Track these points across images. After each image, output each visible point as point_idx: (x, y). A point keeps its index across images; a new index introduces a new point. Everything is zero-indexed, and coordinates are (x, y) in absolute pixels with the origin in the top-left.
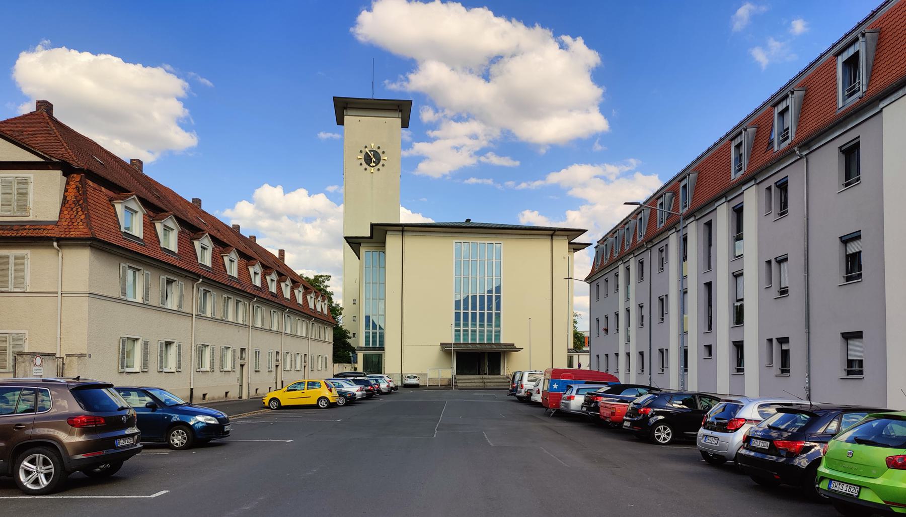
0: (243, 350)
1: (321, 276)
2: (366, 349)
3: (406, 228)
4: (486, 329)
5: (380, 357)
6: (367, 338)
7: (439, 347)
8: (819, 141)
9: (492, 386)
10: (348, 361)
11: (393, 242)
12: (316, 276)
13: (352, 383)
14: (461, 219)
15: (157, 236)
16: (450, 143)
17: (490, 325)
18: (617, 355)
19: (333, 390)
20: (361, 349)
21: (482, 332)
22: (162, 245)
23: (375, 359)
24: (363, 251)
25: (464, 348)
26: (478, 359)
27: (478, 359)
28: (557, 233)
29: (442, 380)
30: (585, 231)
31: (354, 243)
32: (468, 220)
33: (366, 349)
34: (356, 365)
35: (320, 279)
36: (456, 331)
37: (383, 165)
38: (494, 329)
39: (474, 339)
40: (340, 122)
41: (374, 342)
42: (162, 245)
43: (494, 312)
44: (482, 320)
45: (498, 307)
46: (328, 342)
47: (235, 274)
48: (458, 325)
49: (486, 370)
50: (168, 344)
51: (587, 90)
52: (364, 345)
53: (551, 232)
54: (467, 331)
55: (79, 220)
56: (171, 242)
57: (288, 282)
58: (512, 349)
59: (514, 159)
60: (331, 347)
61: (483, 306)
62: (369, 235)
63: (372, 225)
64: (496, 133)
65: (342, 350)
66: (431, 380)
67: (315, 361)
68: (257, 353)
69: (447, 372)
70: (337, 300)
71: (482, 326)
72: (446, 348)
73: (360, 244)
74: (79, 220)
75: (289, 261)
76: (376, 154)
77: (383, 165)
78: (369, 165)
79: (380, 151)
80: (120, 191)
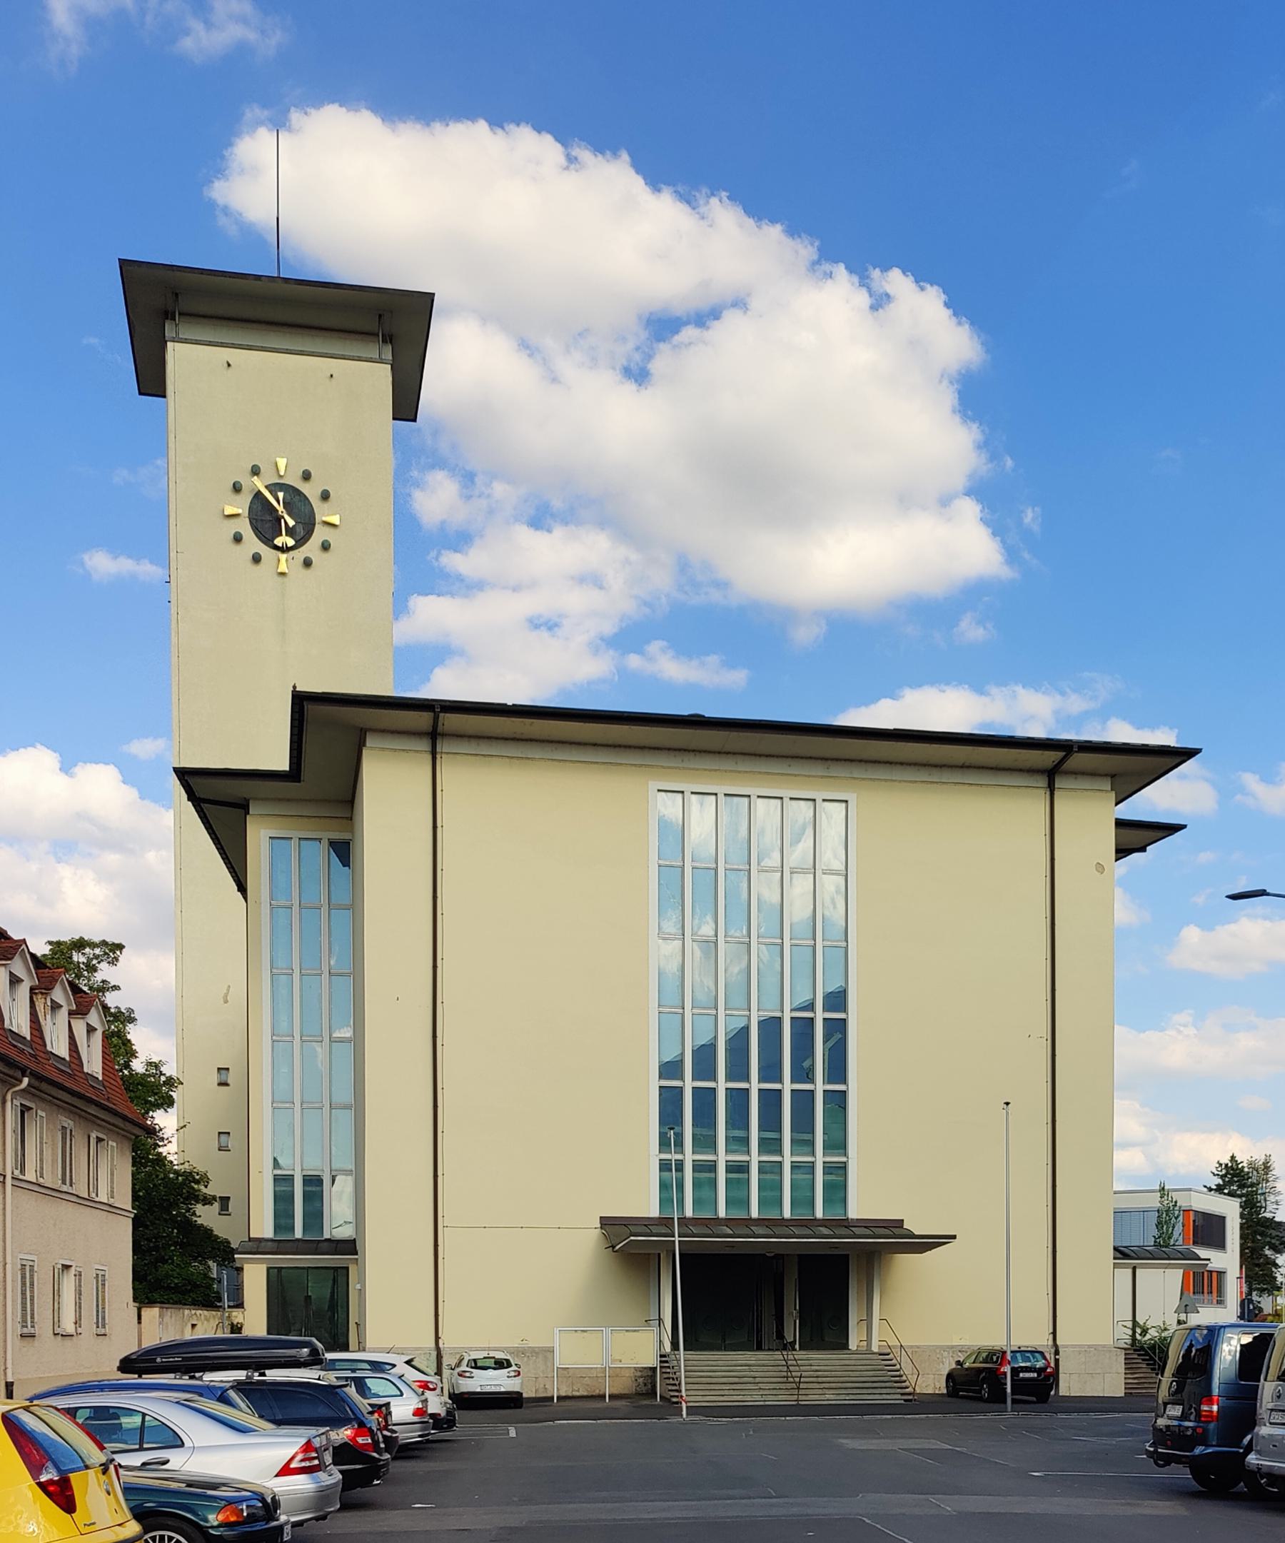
1: (80, 944)
3: (451, 721)
4: (788, 1159)
5: (339, 1277)
6: (283, 1201)
7: (592, 1236)
9: (830, 1398)
10: (204, 1296)
11: (390, 786)
12: (57, 945)
13: (243, 1414)
16: (526, 605)
17: (804, 1141)
19: (89, 1487)
20: (257, 1246)
21: (771, 1171)
23: (319, 1291)
26: (765, 1282)
27: (765, 1282)
28: (1078, 760)
29: (616, 1373)
33: (279, 1245)
34: (237, 1316)
35: (77, 957)
36: (664, 1166)
37: (326, 547)
38: (820, 1159)
39: (738, 1198)
40: (152, 381)
43: (820, 1087)
44: (771, 1119)
45: (837, 1070)
46: (111, 1208)
49: (792, 1331)
51: (950, 445)
52: (268, 1232)
53: (1052, 757)
54: (712, 1167)
59: (730, 664)
60: (123, 1232)
61: (778, 1066)
62: (282, 763)
63: (301, 701)
64: (662, 580)
65: (174, 1244)
69: (636, 1343)
70: (150, 1046)
71: (771, 1145)
72: (631, 1247)
73: (244, 807)
76: (296, 500)
77: (326, 547)
78: (268, 541)
79: (311, 491)
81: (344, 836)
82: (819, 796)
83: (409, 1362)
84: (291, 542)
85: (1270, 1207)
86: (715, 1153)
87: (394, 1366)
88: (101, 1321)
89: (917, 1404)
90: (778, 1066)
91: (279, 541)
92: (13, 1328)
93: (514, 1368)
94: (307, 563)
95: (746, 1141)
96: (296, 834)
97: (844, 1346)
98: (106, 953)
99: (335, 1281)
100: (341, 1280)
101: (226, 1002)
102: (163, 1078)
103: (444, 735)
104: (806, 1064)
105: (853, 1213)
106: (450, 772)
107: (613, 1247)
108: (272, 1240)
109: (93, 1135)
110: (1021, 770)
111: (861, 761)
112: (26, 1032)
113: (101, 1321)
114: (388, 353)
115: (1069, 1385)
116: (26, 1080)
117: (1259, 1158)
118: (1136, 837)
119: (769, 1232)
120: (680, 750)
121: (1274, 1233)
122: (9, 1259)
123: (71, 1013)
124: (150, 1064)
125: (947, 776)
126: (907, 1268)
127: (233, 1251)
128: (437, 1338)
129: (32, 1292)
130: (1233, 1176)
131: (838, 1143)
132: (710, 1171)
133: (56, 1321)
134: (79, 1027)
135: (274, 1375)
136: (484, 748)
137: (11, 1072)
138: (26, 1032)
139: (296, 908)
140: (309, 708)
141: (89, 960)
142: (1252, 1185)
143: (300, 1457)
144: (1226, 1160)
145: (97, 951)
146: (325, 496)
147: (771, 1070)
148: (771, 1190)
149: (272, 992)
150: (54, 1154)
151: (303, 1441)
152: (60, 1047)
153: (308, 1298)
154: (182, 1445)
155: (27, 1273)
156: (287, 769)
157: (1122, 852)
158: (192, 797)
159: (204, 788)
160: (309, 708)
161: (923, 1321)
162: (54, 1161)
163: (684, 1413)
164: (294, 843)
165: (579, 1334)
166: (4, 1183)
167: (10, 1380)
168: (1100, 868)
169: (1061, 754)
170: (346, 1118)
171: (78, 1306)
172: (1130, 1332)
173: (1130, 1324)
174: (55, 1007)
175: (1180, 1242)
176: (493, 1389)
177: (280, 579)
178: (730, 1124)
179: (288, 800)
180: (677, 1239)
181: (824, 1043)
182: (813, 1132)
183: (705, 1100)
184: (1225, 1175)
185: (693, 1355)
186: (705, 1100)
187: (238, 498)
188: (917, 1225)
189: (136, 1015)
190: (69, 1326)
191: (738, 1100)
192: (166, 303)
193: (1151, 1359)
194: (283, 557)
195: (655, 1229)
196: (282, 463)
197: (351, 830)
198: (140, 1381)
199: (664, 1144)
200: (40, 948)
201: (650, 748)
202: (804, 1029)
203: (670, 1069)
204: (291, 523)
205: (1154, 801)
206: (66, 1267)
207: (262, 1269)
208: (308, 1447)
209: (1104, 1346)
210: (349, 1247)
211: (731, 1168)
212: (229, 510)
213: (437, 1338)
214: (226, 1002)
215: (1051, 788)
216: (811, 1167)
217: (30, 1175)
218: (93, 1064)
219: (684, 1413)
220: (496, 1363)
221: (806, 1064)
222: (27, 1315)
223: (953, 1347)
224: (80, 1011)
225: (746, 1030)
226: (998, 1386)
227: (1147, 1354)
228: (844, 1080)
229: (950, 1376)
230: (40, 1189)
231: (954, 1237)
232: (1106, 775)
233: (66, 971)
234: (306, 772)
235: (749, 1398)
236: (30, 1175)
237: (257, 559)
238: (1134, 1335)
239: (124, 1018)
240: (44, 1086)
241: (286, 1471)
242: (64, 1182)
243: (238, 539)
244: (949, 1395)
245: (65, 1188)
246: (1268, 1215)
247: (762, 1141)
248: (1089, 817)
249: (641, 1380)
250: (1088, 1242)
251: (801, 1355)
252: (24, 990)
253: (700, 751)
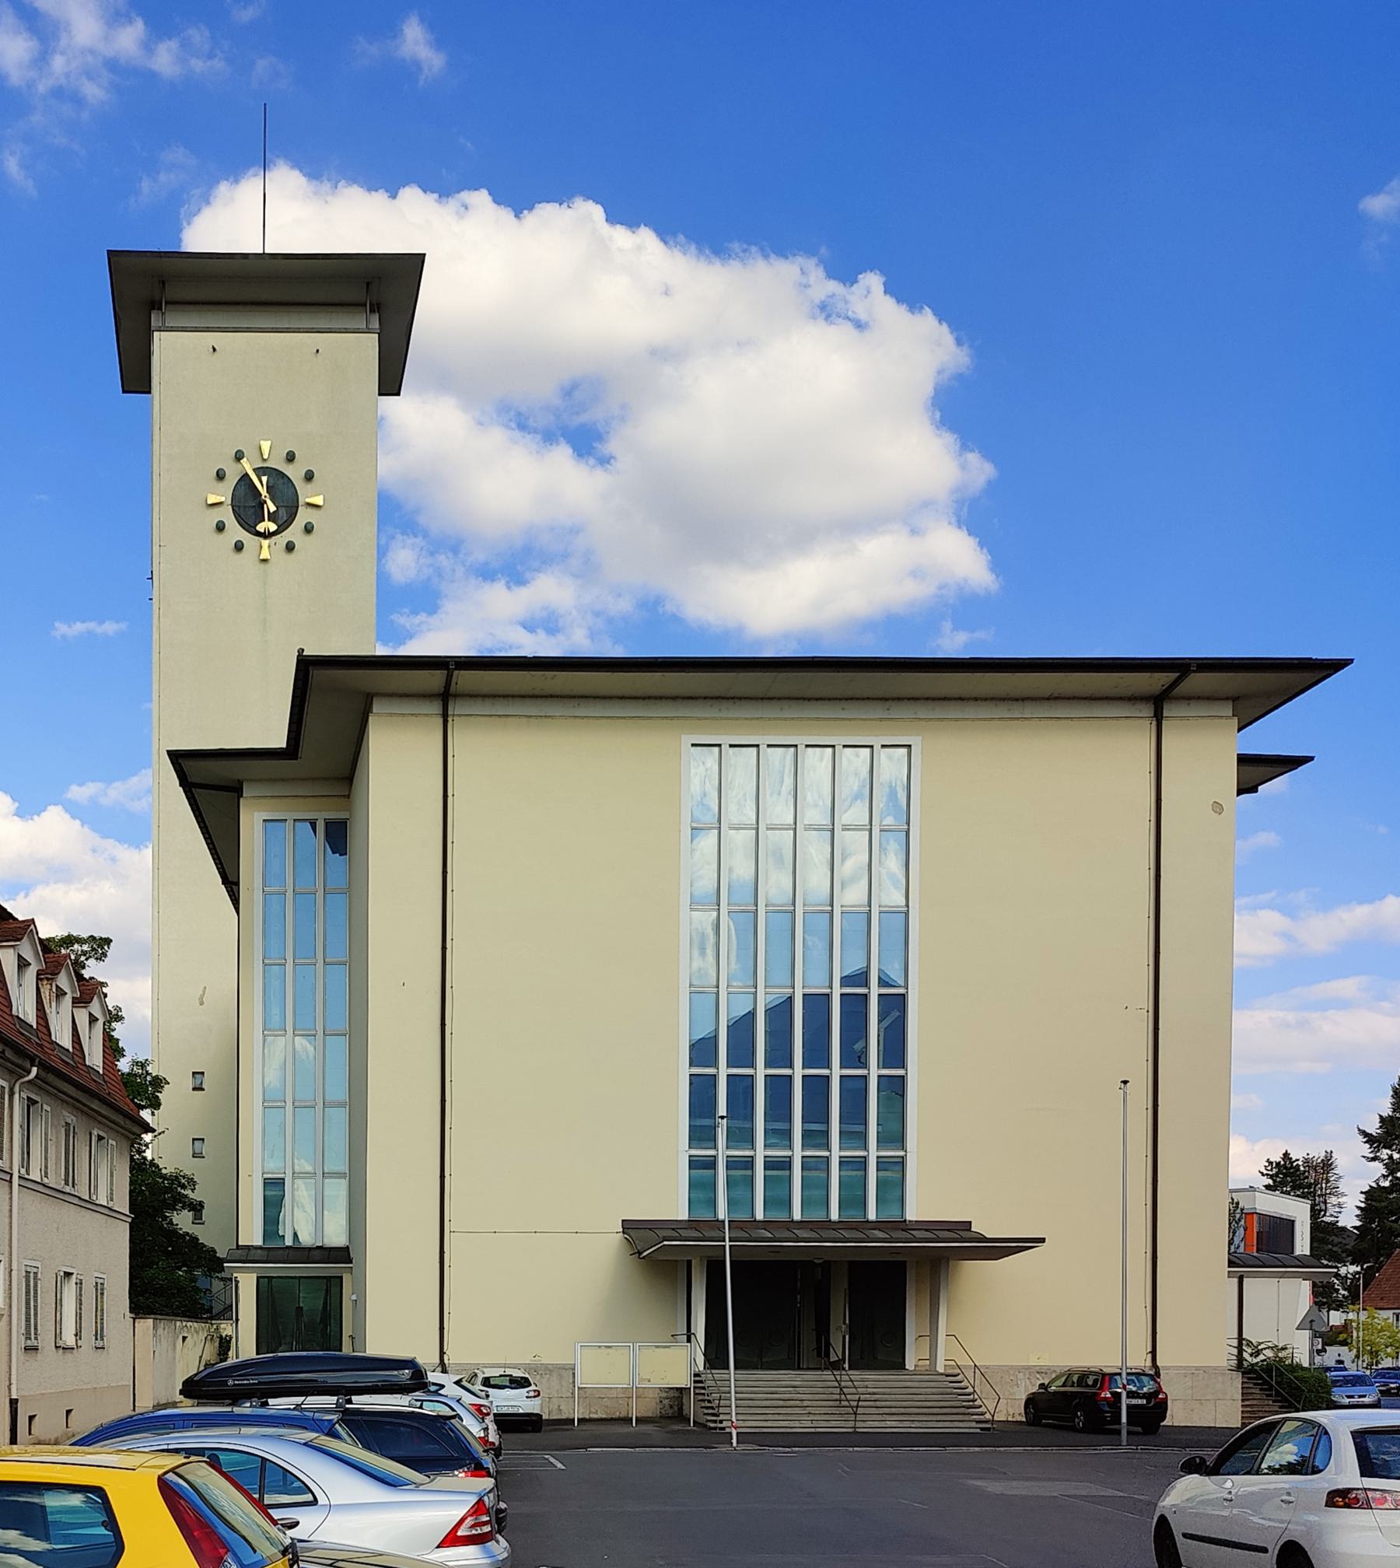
3: (465, 679)
4: (836, 1153)
7: (613, 1239)
9: (892, 1425)
11: (398, 757)
17: (854, 1134)
20: (246, 1255)
21: (816, 1167)
23: (310, 1302)
24: (252, 821)
26: (806, 1289)
27: (806, 1289)
28: (1196, 681)
29: (641, 1393)
30: (1335, 666)
31: (212, 784)
34: (227, 1329)
36: (694, 1164)
38: (873, 1153)
39: (778, 1198)
40: (137, 376)
43: (874, 1072)
44: (817, 1109)
45: (895, 1050)
46: (110, 1212)
48: (701, 1134)
49: (839, 1344)
53: (1158, 681)
54: (749, 1164)
58: (954, 1246)
60: (121, 1234)
61: (820, 1049)
62: (280, 741)
63: (306, 666)
67: (46, 1300)
71: (816, 1137)
72: (659, 1255)
73: (236, 790)
76: (279, 481)
77: (308, 529)
78: (250, 528)
79: (294, 472)
81: (342, 815)
82: (877, 743)
83: (458, 1383)
84: (273, 527)
85: (1331, 1210)
86: (753, 1148)
87: (442, 1386)
88: (99, 1334)
89: (994, 1434)
90: (820, 1049)
91: (261, 528)
92: (18, 1341)
93: (533, 1387)
94: (290, 547)
95: (788, 1134)
96: (290, 816)
97: (901, 1366)
98: (93, 949)
99: (328, 1292)
100: (334, 1290)
101: (202, 1004)
102: (149, 1078)
103: (456, 696)
104: (858, 1046)
105: (911, 1215)
107: (640, 1253)
108: (260, 1248)
109: (95, 1132)
110: (1121, 699)
111: (927, 699)
112: (32, 1019)
113: (99, 1334)
114: (375, 324)
115: (1177, 1416)
116: (34, 1070)
117: (1318, 1154)
118: (1255, 771)
119: (813, 1235)
120: (717, 698)
121: (1336, 1240)
122: (14, 1267)
123: (76, 1002)
124: (136, 1063)
125: (1029, 710)
126: (975, 1276)
127: (222, 1261)
128: (442, 1353)
129: (36, 1301)
130: (1286, 1175)
131: (894, 1135)
132: (746, 1169)
133: (58, 1335)
134: (82, 1017)
135: (361, 1402)
136: (500, 708)
137: (20, 1062)
138: (32, 1019)
139: (290, 894)
140: (317, 675)
141: (78, 956)
142: (1309, 1186)
143: (469, 1521)
144: (1277, 1158)
145: (85, 947)
146: (309, 477)
147: (817, 1053)
148: (816, 1188)
149: (264, 984)
150: (58, 1152)
151: (474, 1499)
152: (66, 1041)
153: (300, 1309)
154: (315, 1502)
155: (31, 1279)
156: (284, 745)
157: (1246, 788)
158: (184, 782)
159: (198, 771)
160: (317, 675)
161: (998, 1338)
162: (58, 1158)
163: (734, 1441)
164: (290, 824)
165: (603, 1350)
166: (11, 1182)
167: (14, 1397)
168: (1218, 808)
169: (1174, 676)
170: (339, 1118)
171: (79, 1316)
172: (1235, 1352)
173: (1235, 1343)
174: (60, 993)
175: (1241, 1250)
176: (511, 1411)
177: (262, 566)
179: (283, 780)
180: (728, 1244)
181: (879, 1021)
182: (865, 1123)
183: (741, 1088)
184: (1277, 1175)
185: (744, 1374)
186: (741, 1088)
187: (221, 485)
188: (988, 1226)
189: (123, 1014)
190: (69, 1339)
191: (779, 1088)
192: (157, 289)
193: (1265, 1382)
194: (265, 543)
195: (684, 1233)
196: (266, 446)
197: (349, 808)
198: (237, 1410)
200: (47, 930)
201: (684, 698)
202: (855, 1007)
203: (702, 1051)
204: (273, 508)
205: (1270, 735)
206: (68, 1275)
208: (479, 1508)
209: (1215, 1368)
210: (342, 1255)
211: (769, 1165)
212: (212, 499)
213: (442, 1353)
214: (202, 1004)
215: (1159, 718)
216: (863, 1163)
217: (35, 1175)
218: (95, 1058)
219: (734, 1441)
220: (511, 1381)
221: (858, 1046)
222: (30, 1328)
223: (1028, 1368)
224: (81, 1001)
225: (752, 1015)
226: (1079, 1411)
227: (1260, 1377)
228: (902, 1064)
229: (1031, 1401)
230: (44, 1189)
231: (1043, 1240)
232: (1227, 699)
233: (65, 961)
234: (304, 750)
235: (797, 1424)
237: (239, 547)
238: (1240, 1358)
239: (115, 1016)
240: (51, 1078)
241: (451, 1540)
242: (67, 1183)
243: (220, 527)
244: (1028, 1423)
245: (68, 1189)
246: (1327, 1219)
247: (806, 1135)
248: (1204, 750)
249: (666, 1402)
250: (1199, 1245)
251: (855, 1375)
252: (31, 973)
253: (740, 698)
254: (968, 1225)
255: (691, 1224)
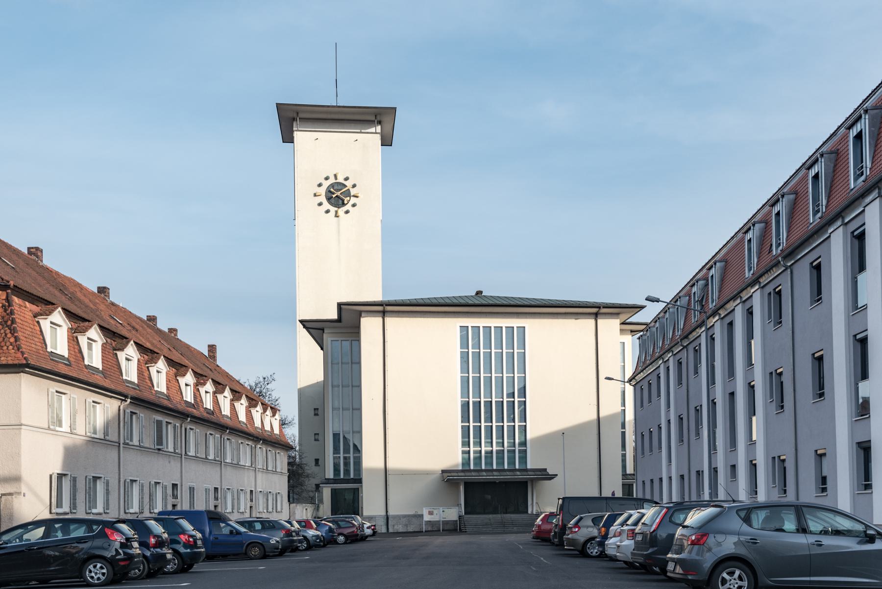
0: (175, 486)
2: (335, 481)
3: (389, 308)
8: (802, 251)
11: (370, 326)
14: (467, 291)
15: (81, 352)
18: (661, 479)
20: (328, 481)
22: (86, 363)
24: (327, 338)
25: (474, 477)
32: (479, 293)
33: (335, 481)
36: (463, 452)
40: (288, 138)
41: (347, 472)
42: (86, 363)
45: (524, 418)
47: (163, 389)
50: (96, 479)
53: (595, 310)
55: (8, 344)
56: (94, 358)
57: (227, 393)
66: (429, 523)
68: (192, 490)
72: (448, 479)
74: (8, 344)
75: (222, 361)
80: (46, 305)
97: (527, 512)
105: (529, 467)
106: (388, 320)
158: (304, 327)
167: (824, 475)
178: (486, 438)
188: (550, 472)
199: (463, 444)
207: (329, 490)
236: (135, 442)
254: (545, 470)
255: (462, 471)
